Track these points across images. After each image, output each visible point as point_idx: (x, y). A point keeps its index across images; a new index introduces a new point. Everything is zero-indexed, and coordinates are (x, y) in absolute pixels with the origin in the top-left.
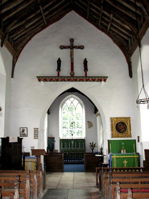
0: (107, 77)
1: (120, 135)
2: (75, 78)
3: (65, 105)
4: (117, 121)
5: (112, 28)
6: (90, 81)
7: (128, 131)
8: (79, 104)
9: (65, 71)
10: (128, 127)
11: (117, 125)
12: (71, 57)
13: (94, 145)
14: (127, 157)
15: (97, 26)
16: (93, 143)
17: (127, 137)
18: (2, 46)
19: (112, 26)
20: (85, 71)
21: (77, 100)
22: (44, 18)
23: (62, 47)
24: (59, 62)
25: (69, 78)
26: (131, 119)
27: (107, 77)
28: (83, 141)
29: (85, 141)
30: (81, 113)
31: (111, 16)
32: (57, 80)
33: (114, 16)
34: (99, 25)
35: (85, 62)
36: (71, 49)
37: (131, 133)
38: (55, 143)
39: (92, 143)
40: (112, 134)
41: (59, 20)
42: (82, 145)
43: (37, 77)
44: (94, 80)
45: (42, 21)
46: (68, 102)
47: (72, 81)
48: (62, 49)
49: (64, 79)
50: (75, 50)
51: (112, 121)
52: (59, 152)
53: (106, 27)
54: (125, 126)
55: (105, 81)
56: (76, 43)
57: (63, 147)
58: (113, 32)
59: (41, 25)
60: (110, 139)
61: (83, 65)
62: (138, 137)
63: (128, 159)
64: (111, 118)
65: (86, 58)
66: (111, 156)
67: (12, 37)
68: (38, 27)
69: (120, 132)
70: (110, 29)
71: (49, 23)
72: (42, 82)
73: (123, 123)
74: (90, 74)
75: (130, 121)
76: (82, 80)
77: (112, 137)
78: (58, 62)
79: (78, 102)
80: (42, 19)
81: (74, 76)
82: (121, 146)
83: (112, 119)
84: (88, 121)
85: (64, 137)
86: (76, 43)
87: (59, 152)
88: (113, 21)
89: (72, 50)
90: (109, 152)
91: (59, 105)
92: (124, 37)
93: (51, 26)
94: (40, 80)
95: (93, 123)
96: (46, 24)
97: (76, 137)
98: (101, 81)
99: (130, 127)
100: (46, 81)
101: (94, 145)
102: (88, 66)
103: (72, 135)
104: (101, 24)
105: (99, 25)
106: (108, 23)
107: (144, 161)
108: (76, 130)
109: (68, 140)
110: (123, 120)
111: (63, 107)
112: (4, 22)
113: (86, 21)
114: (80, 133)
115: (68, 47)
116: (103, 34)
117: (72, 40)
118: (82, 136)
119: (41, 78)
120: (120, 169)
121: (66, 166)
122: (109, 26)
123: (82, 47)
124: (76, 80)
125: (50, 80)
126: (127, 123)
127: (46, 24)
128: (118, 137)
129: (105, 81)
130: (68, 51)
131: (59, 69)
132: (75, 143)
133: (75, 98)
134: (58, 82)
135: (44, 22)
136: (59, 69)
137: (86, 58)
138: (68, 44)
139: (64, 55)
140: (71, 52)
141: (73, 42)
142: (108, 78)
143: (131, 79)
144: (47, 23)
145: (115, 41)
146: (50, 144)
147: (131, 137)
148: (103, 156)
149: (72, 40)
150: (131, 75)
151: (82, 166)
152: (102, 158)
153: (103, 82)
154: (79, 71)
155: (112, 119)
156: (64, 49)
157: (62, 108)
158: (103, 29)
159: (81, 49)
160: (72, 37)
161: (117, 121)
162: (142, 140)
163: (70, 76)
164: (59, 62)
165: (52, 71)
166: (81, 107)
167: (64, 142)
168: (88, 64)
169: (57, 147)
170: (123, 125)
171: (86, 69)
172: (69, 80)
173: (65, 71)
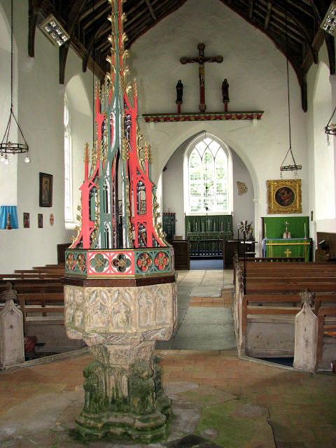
0: (263, 112)
1: (282, 208)
2: (207, 115)
3: (194, 151)
4: (278, 187)
5: (272, 23)
6: (234, 119)
7: (296, 203)
8: (221, 149)
9: (191, 103)
10: (297, 196)
11: (278, 192)
12: (200, 77)
13: (249, 226)
14: (291, 244)
15: (247, 19)
16: (246, 222)
17: (295, 212)
18: (84, 70)
19: (272, 19)
20: (224, 102)
21: (219, 142)
22: (151, 10)
23: (185, 61)
24: (180, 87)
25: (197, 115)
26: (302, 183)
27: (263, 112)
28: (228, 219)
29: (62, 245)
30: (225, 167)
31: (269, 6)
32: (177, 120)
33: (273, 6)
34: (251, 16)
35: (225, 87)
36: (200, 63)
37: (300, 206)
38: (177, 223)
39: (244, 222)
40: (269, 208)
41: (177, 9)
42: (227, 226)
43: (143, 115)
44: (239, 118)
45: (147, 16)
46: (200, 146)
47: (202, 120)
48: (185, 63)
49: (188, 117)
50: (207, 64)
51: (269, 187)
52: (184, 239)
53: (263, 21)
54: (291, 193)
55: (259, 118)
56: (208, 52)
57: (192, 231)
58: (275, 28)
59: (146, 22)
60: (266, 215)
61: (221, 91)
62: (312, 212)
63: (292, 248)
64: (268, 181)
65: (226, 80)
66: (266, 242)
67: (98, 49)
68: (143, 25)
69: (282, 205)
70: (270, 24)
71: (160, 16)
72: (152, 124)
73: (288, 190)
74: (232, 105)
75: (300, 186)
76: (220, 118)
77: (270, 211)
78: (177, 87)
79: (219, 146)
80: (148, 11)
81: (206, 111)
82: (284, 226)
83: (269, 184)
84: (238, 182)
85: (193, 212)
86: (208, 52)
87: (184, 239)
88: (272, 12)
89: (202, 66)
90: (263, 238)
91: (183, 153)
92: (294, 38)
93: (163, 20)
94: (147, 120)
95: (248, 186)
96: (155, 18)
97: (216, 210)
98: (251, 118)
99: (300, 196)
100: (159, 121)
101: (249, 226)
102: (229, 93)
103: (207, 209)
104: (254, 14)
105: (251, 16)
106: (265, 14)
107: (316, 250)
108: (71, 291)
109: (200, 217)
110: (288, 185)
111: (191, 155)
112: (86, 30)
113: (227, 8)
114: (222, 204)
115: (196, 60)
116: (258, 31)
117: (201, 47)
118: (228, 210)
119: (149, 117)
120: (280, 260)
121: (192, 263)
122: (267, 20)
123: (218, 59)
124: (209, 119)
125: (165, 120)
126: (296, 190)
127: (155, 18)
128: (279, 212)
129: (259, 118)
130: (195, 66)
131: (179, 99)
132: (213, 223)
133: (214, 139)
134: (179, 123)
135: (151, 16)
136: (179, 99)
137: (226, 80)
138: (194, 52)
139: (187, 73)
140: (200, 68)
141: (203, 50)
142: (264, 115)
143: (305, 114)
144: (156, 16)
145: (278, 46)
146: (167, 225)
147: (301, 212)
148: (254, 243)
149: (201, 47)
150: (305, 106)
151: (221, 262)
152: (252, 247)
153: (255, 121)
154: (214, 102)
155: (269, 184)
156: (188, 64)
157: (188, 157)
158: (257, 22)
159: (218, 62)
160: (201, 42)
161: (278, 187)
162: (317, 217)
163: (199, 111)
164: (180, 87)
165: (165, 103)
166: (224, 154)
167: (192, 221)
168: (229, 89)
169: (181, 231)
170: (288, 193)
171: (226, 98)
172: (197, 119)
173: (191, 103)
